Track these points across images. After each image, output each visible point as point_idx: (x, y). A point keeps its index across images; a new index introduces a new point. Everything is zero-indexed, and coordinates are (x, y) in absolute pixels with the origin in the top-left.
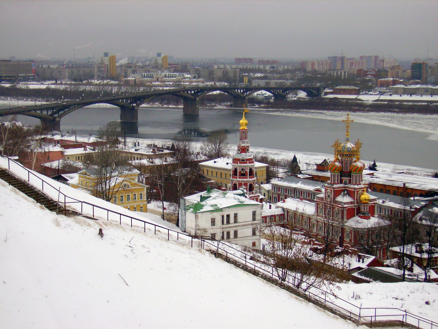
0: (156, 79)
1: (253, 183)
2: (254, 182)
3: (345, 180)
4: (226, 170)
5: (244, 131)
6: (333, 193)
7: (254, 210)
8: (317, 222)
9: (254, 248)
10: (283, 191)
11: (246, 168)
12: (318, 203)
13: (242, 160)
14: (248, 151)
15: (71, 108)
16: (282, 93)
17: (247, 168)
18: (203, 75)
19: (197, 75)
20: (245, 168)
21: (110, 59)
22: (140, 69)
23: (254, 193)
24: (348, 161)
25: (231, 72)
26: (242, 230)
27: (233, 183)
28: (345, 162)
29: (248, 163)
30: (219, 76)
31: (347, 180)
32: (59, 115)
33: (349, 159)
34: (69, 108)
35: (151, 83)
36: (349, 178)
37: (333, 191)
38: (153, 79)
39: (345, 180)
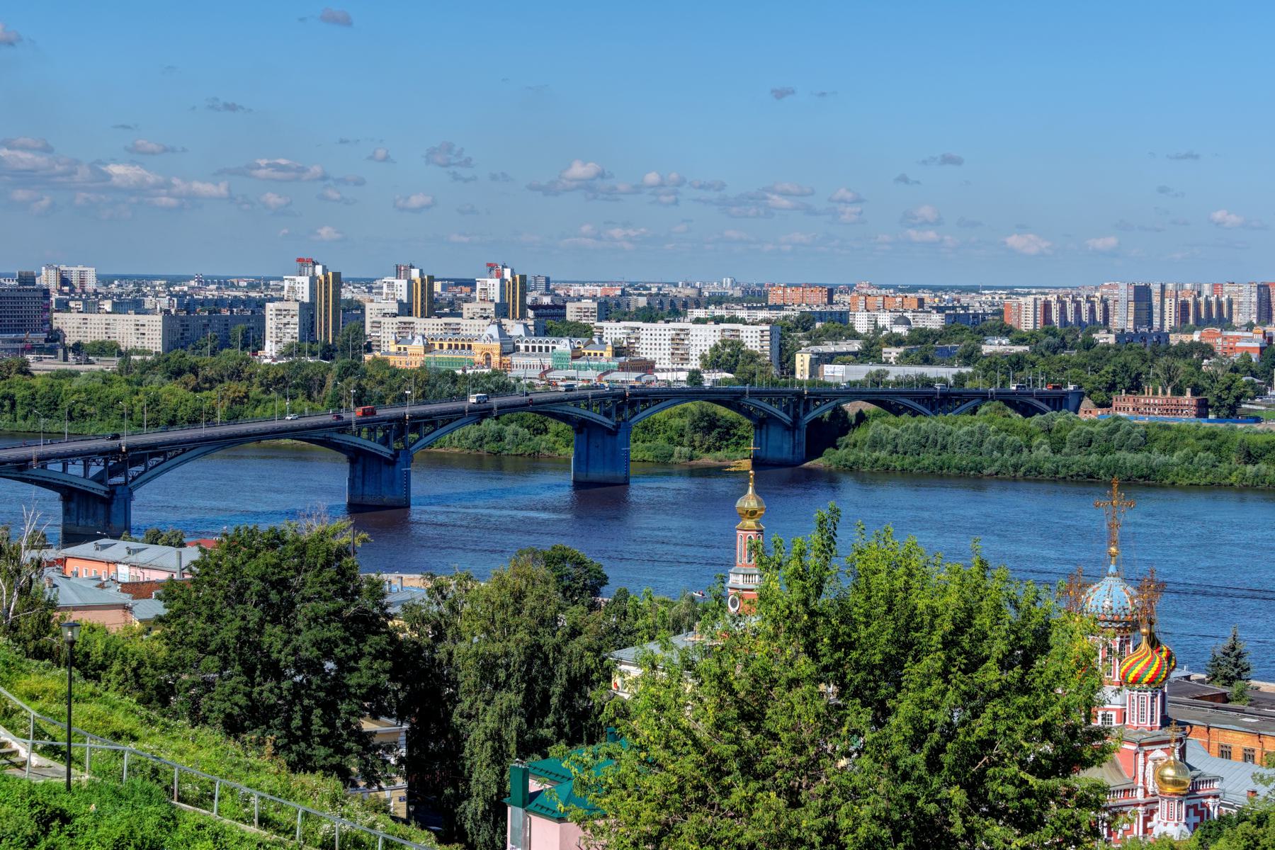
0: (479, 358)
15: (169, 454)
32: (126, 479)
34: (165, 457)
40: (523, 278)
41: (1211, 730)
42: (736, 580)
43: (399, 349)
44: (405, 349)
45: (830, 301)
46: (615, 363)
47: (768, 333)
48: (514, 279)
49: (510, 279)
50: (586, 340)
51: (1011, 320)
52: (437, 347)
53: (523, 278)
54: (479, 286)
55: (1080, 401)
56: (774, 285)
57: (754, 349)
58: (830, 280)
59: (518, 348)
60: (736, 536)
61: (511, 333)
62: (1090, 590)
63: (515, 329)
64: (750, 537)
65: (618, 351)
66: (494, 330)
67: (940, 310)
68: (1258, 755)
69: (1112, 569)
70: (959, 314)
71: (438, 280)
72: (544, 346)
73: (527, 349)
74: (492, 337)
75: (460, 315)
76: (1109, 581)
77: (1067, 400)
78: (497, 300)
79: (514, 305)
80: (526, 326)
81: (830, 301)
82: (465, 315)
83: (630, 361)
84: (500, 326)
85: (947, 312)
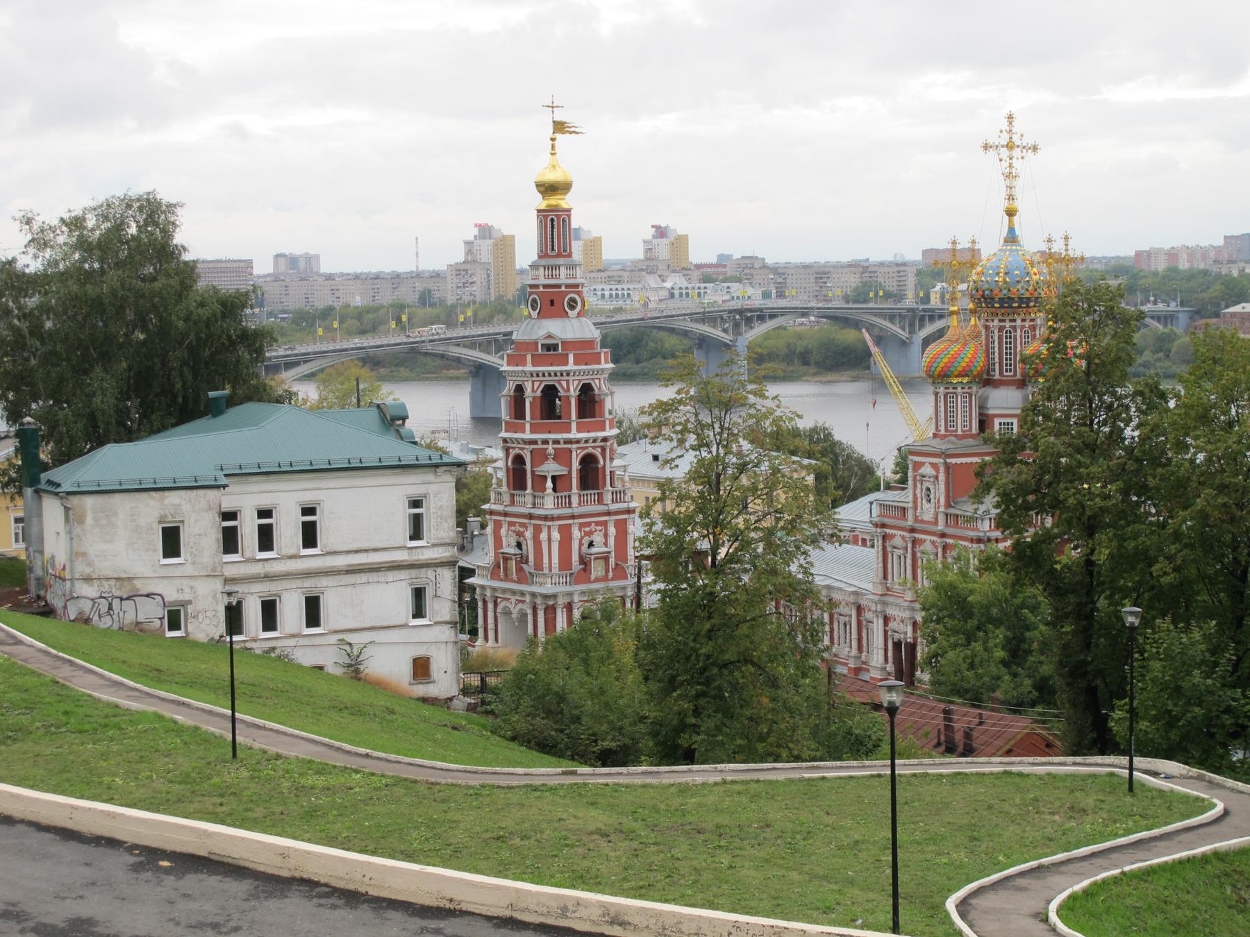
1: (598, 452)
2: (603, 449)
3: (1003, 420)
4: (643, 481)
5: (552, 215)
6: (942, 477)
7: (415, 491)
8: (859, 609)
9: (421, 690)
11: (564, 384)
12: (888, 531)
13: (548, 347)
14: (572, 308)
17: (568, 381)
19: (777, 288)
20: (559, 381)
21: (496, 245)
22: (593, 275)
23: (608, 498)
24: (1015, 331)
26: (349, 589)
27: (512, 453)
28: (1000, 338)
29: (571, 358)
31: (1009, 420)
33: (1019, 322)
37: (942, 469)
39: (1003, 420)
57: (891, 289)
77: (1177, 318)
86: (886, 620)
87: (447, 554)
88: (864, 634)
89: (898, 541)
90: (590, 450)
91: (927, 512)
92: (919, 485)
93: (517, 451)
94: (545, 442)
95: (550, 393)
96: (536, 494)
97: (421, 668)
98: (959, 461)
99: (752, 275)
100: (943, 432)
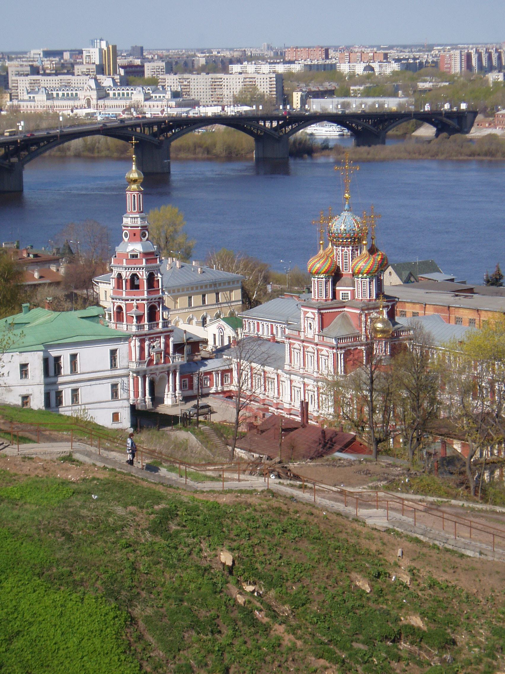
0: (83, 102)
1: (156, 304)
3: (343, 292)
6: (317, 318)
10: (252, 327)
11: (141, 273)
13: (133, 256)
16: (372, 128)
18: (196, 91)
25: (262, 80)
27: (116, 305)
30: (235, 91)
31: (347, 292)
35: (72, 111)
36: (352, 288)
38: (77, 103)
40: (114, 47)
41: (451, 308)
42: (127, 221)
43: (30, 97)
44: (34, 97)
45: (327, 57)
46: (173, 103)
47: (275, 79)
48: (108, 48)
49: (106, 49)
50: (153, 87)
51: (444, 67)
52: (55, 96)
53: (114, 47)
54: (85, 54)
55: (475, 117)
56: (349, 49)
58: (326, 44)
59: (108, 95)
60: (126, 194)
61: (104, 85)
62: (333, 221)
63: (107, 82)
64: (134, 196)
65: (176, 95)
66: (92, 83)
67: (397, 60)
68: (477, 321)
69: (346, 207)
70: (410, 63)
71: (66, 51)
72: (125, 92)
73: (114, 94)
74: (90, 87)
75: (73, 74)
76: (345, 214)
78: (97, 63)
79: (109, 66)
80: (114, 80)
81: (327, 57)
82: (76, 73)
83: (183, 100)
84: (96, 79)
85: (403, 62)
86: (291, 381)
87: (126, 372)
88: (281, 387)
89: (296, 346)
90: (153, 303)
91: (310, 334)
92: (306, 321)
93: (119, 304)
94: (133, 300)
95: (134, 276)
96: (128, 324)
97: (116, 417)
98: (326, 311)
99: (165, 79)
100: (317, 298)
